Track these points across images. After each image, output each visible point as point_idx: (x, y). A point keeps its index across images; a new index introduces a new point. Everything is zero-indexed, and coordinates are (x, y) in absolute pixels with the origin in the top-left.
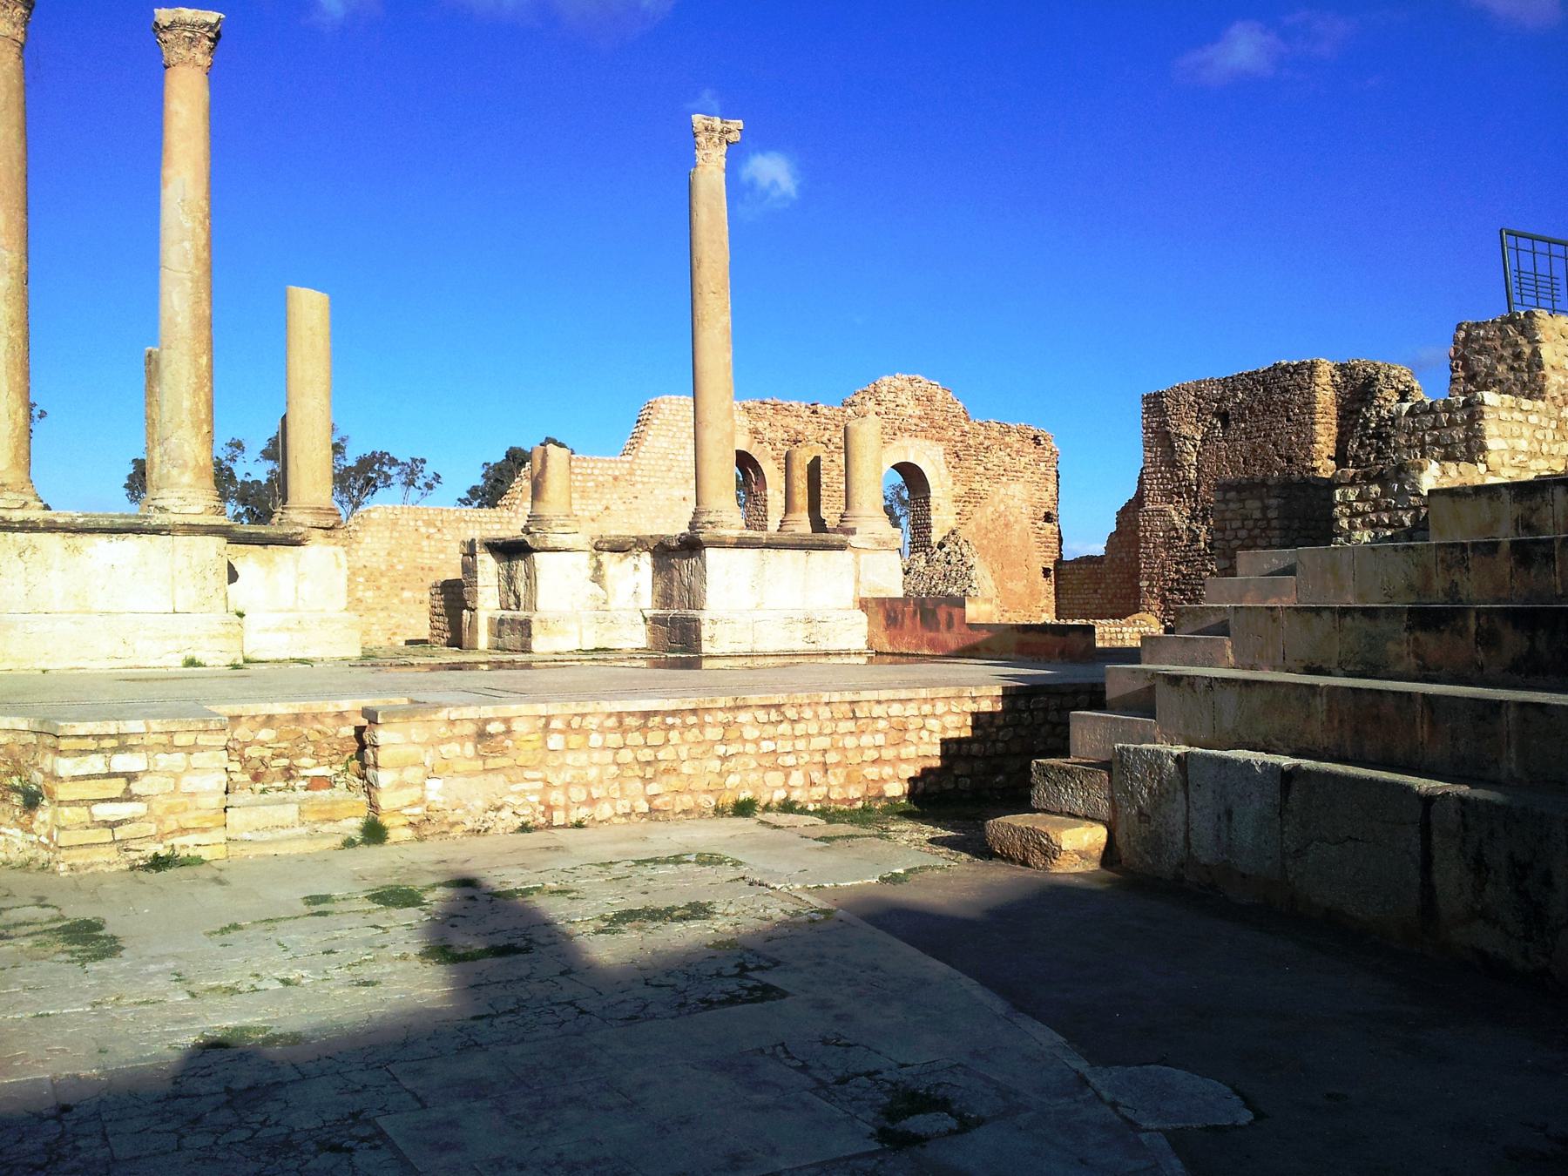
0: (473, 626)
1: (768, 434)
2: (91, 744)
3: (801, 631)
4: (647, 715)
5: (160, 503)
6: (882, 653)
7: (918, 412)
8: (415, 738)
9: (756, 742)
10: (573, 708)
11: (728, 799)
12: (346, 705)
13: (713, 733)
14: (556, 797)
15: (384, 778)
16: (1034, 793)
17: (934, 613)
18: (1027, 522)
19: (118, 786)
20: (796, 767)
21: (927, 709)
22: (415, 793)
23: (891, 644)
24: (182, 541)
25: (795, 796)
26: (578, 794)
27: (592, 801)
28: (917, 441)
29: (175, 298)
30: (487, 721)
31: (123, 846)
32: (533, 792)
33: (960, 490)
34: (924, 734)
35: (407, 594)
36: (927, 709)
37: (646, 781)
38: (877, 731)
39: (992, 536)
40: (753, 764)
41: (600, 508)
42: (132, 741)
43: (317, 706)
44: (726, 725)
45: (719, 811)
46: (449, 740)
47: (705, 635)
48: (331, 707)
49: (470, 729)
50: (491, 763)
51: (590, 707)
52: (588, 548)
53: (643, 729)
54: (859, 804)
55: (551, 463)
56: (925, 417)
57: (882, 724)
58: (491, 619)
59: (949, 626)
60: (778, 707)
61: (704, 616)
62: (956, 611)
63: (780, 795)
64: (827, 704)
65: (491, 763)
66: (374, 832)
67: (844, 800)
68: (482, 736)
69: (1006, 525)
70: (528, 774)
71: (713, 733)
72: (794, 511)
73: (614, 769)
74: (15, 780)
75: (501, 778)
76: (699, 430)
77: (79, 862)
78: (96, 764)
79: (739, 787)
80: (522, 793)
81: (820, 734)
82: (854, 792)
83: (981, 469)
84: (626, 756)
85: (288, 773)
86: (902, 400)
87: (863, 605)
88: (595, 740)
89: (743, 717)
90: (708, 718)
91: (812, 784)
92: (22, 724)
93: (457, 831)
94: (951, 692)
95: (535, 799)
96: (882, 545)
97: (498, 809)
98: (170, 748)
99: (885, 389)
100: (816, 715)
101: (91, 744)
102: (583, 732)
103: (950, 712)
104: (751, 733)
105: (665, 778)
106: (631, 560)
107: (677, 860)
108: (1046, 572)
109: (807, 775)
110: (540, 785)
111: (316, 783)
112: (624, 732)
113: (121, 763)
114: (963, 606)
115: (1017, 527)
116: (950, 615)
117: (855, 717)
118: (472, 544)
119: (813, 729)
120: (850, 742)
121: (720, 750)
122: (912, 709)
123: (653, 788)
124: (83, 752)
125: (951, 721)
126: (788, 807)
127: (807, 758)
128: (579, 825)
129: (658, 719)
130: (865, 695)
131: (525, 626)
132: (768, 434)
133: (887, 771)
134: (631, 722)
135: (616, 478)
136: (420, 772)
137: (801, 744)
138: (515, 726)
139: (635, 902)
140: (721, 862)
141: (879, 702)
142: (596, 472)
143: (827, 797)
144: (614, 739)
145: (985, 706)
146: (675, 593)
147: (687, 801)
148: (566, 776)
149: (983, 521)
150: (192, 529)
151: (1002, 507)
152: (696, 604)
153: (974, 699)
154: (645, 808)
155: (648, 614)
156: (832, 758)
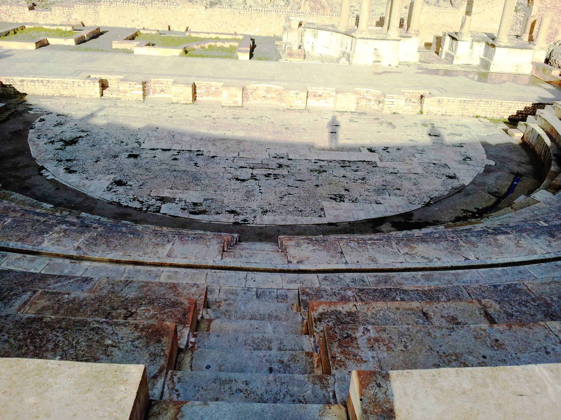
0: (442, 51)
11: (475, 115)
12: (420, 91)
14: (448, 111)
15: (424, 105)
19: (391, 103)
24: (392, 42)
26: (451, 111)
27: (453, 112)
31: (390, 110)
35: (428, 31)
43: (416, 91)
45: (473, 117)
47: (491, 67)
53: (464, 103)
55: (467, 21)
58: (446, 52)
61: (492, 63)
66: (421, 112)
78: (389, 100)
82: (498, 117)
84: (460, 106)
85: (410, 100)
87: (533, 63)
89: (481, 103)
92: (380, 92)
96: (542, 48)
104: (482, 105)
106: (480, 44)
107: (462, 126)
111: (414, 102)
113: (392, 100)
118: (445, 34)
120: (500, 109)
122: (513, 104)
125: (520, 107)
126: (485, 117)
131: (453, 57)
133: (505, 114)
139: (453, 132)
144: (459, 104)
147: (468, 114)
150: (394, 40)
152: (491, 59)
155: (482, 57)
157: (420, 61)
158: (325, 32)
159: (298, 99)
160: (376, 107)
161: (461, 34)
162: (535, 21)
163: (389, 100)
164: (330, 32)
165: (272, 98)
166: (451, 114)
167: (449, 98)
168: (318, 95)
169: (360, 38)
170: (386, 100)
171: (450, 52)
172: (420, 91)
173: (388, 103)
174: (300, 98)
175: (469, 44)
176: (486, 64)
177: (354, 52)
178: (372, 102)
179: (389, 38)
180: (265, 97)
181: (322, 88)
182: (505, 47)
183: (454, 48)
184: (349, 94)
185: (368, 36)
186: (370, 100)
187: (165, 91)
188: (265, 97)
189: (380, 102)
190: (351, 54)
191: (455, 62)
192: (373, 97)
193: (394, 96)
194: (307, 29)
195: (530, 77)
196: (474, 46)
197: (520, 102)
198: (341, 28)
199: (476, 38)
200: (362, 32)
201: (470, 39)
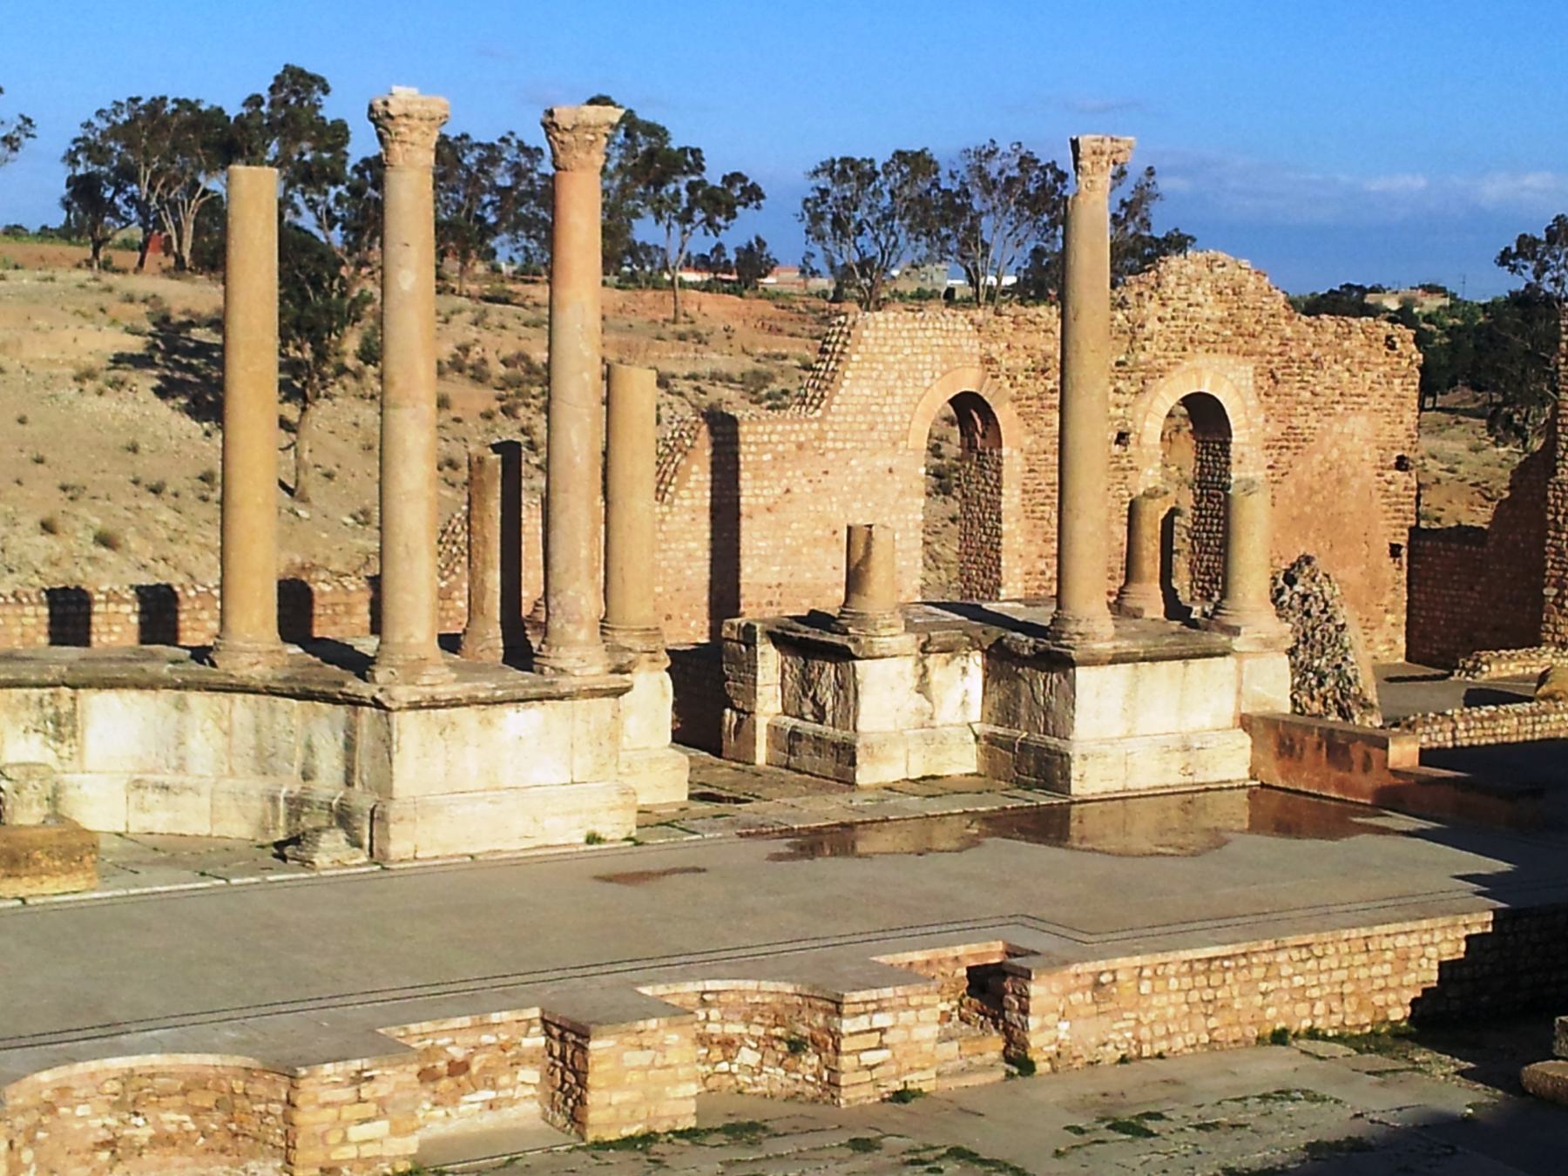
1: (1006, 362)
2: (861, 1008)
3: (1177, 761)
4: (1210, 960)
5: (559, 665)
6: (1270, 787)
7: (1220, 312)
8: (1054, 990)
9: (1289, 978)
10: (1160, 958)
13: (1258, 972)
14: (1145, 1033)
16: (1556, 1044)
17: (1345, 750)
20: (1319, 999)
21: (1427, 938)
22: (1051, 1034)
23: (1284, 777)
24: (581, 703)
25: (1319, 1023)
26: (1160, 1030)
27: (1169, 1035)
28: (1215, 359)
29: (574, 438)
30: (1101, 973)
31: (876, 1083)
32: (1128, 1029)
33: (1274, 430)
34: (1424, 961)
36: (1427, 938)
37: (1207, 1016)
38: (1385, 962)
39: (1318, 498)
40: (1287, 998)
41: (778, 491)
42: (885, 1004)
44: (1268, 965)
46: (1076, 989)
48: (950, 952)
49: (1090, 980)
50: (1103, 1008)
51: (1171, 956)
52: (915, 651)
54: (1368, 1029)
56: (1230, 320)
57: (1389, 955)
58: (774, 730)
59: (1366, 767)
60: (1307, 946)
61: (1075, 752)
62: (1375, 752)
63: (1307, 1023)
64: (1347, 940)
65: (1103, 1008)
67: (1357, 1026)
68: (1098, 985)
69: (1339, 481)
70: (1126, 1015)
71: (1258, 972)
72: (1140, 580)
73: (1185, 1008)
74: (779, 1031)
75: (1108, 1019)
76: (1067, 516)
77: (852, 1096)
78: (863, 1023)
79: (1276, 1019)
80: (1120, 1031)
81: (1340, 968)
82: (1365, 1018)
83: (1306, 395)
86: (1198, 295)
87: (1245, 723)
88: (1174, 983)
89: (1282, 957)
90: (1255, 960)
91: (1331, 1012)
92: (789, 989)
93: (1078, 1064)
94: (1447, 921)
95: (1129, 1035)
96: (1268, 644)
97: (1105, 1044)
98: (907, 1007)
99: (1172, 279)
100: (1337, 950)
101: (861, 1008)
102: (1165, 977)
103: (1446, 940)
104: (1286, 970)
105: (1221, 1013)
108: (1395, 550)
109: (1328, 1005)
110: (1132, 1023)
112: (1193, 977)
113: (880, 1020)
114: (1386, 748)
115: (1356, 483)
116: (1368, 756)
117: (1368, 951)
119: (1334, 965)
120: (1363, 973)
121: (1263, 986)
122: (1414, 940)
123: (1213, 1022)
124: (857, 1015)
127: (1328, 989)
128: (1160, 1056)
129: (1217, 963)
130: (1378, 929)
132: (1006, 362)
133: (1392, 997)
134: (1199, 967)
135: (800, 446)
136: (1056, 1017)
137: (1324, 978)
138: (1119, 977)
140: (1324, 1100)
141: (1388, 935)
142: (775, 438)
143: (1343, 1023)
144: (1187, 982)
145: (1476, 930)
146: (1023, 711)
147: (1236, 1032)
148: (1152, 1016)
149: (1307, 478)
150: (594, 693)
151: (1335, 453)
153: (1466, 926)
154: (1205, 1039)
156: (1348, 988)
157: (691, 797)
158: (133, 694)
159: (371, 1109)
160: (776, 1078)
161: (860, 619)
162: (1174, 512)
163: (863, 1023)
165: (163, 1140)
166: (1162, 1046)
167: (1138, 960)
168: (442, 1065)
169: (415, 706)
170: (847, 1026)
171: (809, 727)
172: (961, 950)
173: (858, 1043)
174: (381, 1102)
175: (907, 667)
176: (1043, 765)
177: (384, 788)
178: (748, 1057)
181: (466, 1021)
182: (1116, 659)
183: (828, 699)
184: (652, 1023)
185: (460, 690)
186: (728, 1044)
189: (796, 1047)
190: (362, 800)
191: (866, 775)
192: (748, 1021)
193: (887, 992)
195: (1252, 794)
196: (935, 676)
197: (1441, 921)
198: (245, 659)
199: (939, 636)
200: (413, 670)
201: (909, 642)
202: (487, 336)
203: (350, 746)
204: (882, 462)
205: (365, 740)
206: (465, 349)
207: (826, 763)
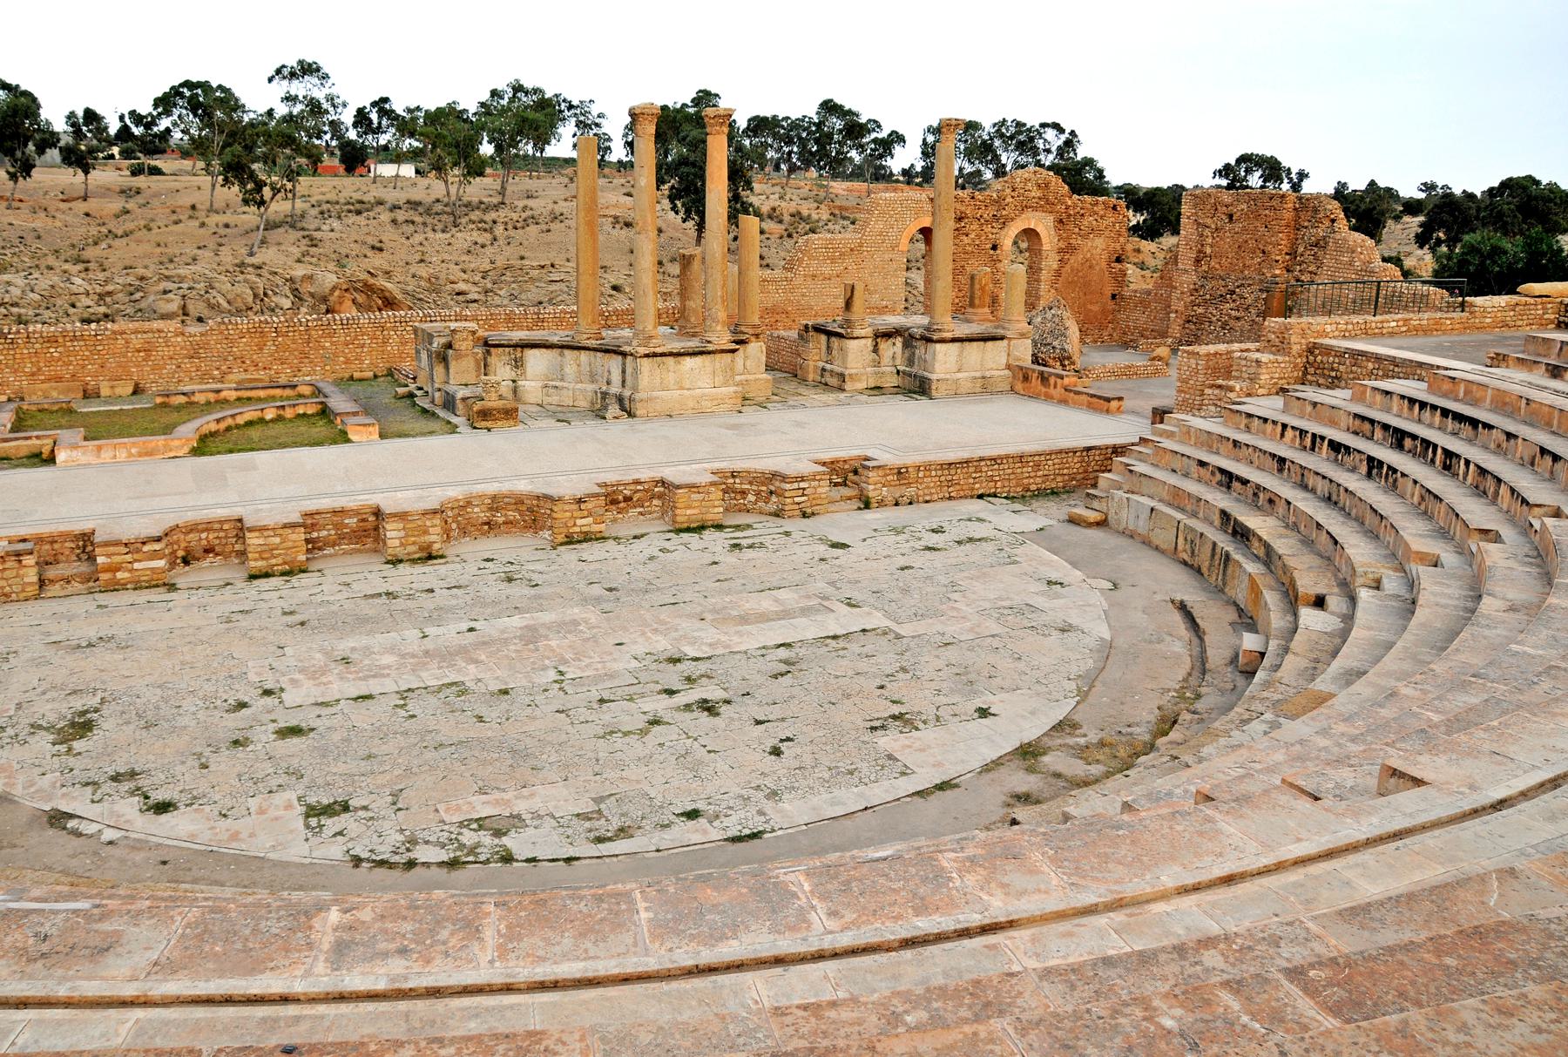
7: (1039, 194)
18: (1104, 265)
24: (718, 356)
33: (1062, 245)
68: (899, 473)
78: (796, 485)
106: (892, 340)
113: (802, 485)
118: (806, 326)
150: (723, 351)
164: (556, 352)
169: (647, 356)
177: (635, 389)
179: (711, 347)
180: (488, 523)
185: (676, 346)
186: (744, 493)
187: (217, 549)
188: (488, 523)
190: (627, 393)
194: (492, 350)
202: (783, 204)
203: (624, 372)
204: (887, 257)
205: (629, 370)
206: (774, 209)
207: (833, 381)
